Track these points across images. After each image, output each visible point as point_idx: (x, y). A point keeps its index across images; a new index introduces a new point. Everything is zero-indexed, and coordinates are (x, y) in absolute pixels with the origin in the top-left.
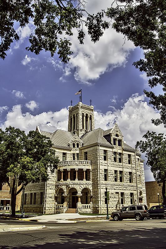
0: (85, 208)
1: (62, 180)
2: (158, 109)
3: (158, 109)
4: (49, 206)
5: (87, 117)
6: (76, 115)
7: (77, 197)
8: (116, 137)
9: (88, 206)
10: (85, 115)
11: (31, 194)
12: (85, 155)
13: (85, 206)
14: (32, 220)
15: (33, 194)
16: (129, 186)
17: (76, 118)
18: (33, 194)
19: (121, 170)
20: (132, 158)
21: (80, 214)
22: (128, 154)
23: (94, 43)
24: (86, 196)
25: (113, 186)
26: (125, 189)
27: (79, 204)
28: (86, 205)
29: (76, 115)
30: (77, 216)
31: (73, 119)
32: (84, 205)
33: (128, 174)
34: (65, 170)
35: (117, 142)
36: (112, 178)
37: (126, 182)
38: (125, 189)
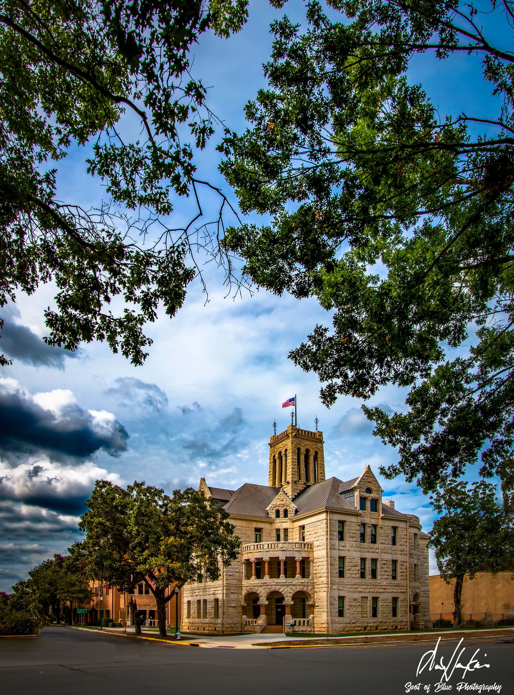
0: (300, 625)
1: (253, 577)
2: (394, 445)
3: (394, 445)
4: (231, 622)
5: (307, 457)
6: (283, 453)
7: (259, 606)
8: (366, 495)
9: (306, 622)
10: (303, 451)
11: (199, 601)
12: (300, 531)
13: (300, 621)
14: (191, 645)
15: (202, 602)
16: (360, 584)
17: (284, 458)
18: (202, 602)
19: (374, 556)
20: (400, 533)
21: (288, 635)
22: (392, 527)
23: (171, 317)
24: (302, 604)
25: (356, 586)
26: (382, 590)
27: (288, 619)
28: (302, 620)
29: (283, 453)
30: (282, 638)
31: (278, 462)
32: (298, 620)
33: (391, 563)
34: (260, 561)
35: (368, 504)
36: (355, 572)
37: (383, 577)
38: (382, 590)
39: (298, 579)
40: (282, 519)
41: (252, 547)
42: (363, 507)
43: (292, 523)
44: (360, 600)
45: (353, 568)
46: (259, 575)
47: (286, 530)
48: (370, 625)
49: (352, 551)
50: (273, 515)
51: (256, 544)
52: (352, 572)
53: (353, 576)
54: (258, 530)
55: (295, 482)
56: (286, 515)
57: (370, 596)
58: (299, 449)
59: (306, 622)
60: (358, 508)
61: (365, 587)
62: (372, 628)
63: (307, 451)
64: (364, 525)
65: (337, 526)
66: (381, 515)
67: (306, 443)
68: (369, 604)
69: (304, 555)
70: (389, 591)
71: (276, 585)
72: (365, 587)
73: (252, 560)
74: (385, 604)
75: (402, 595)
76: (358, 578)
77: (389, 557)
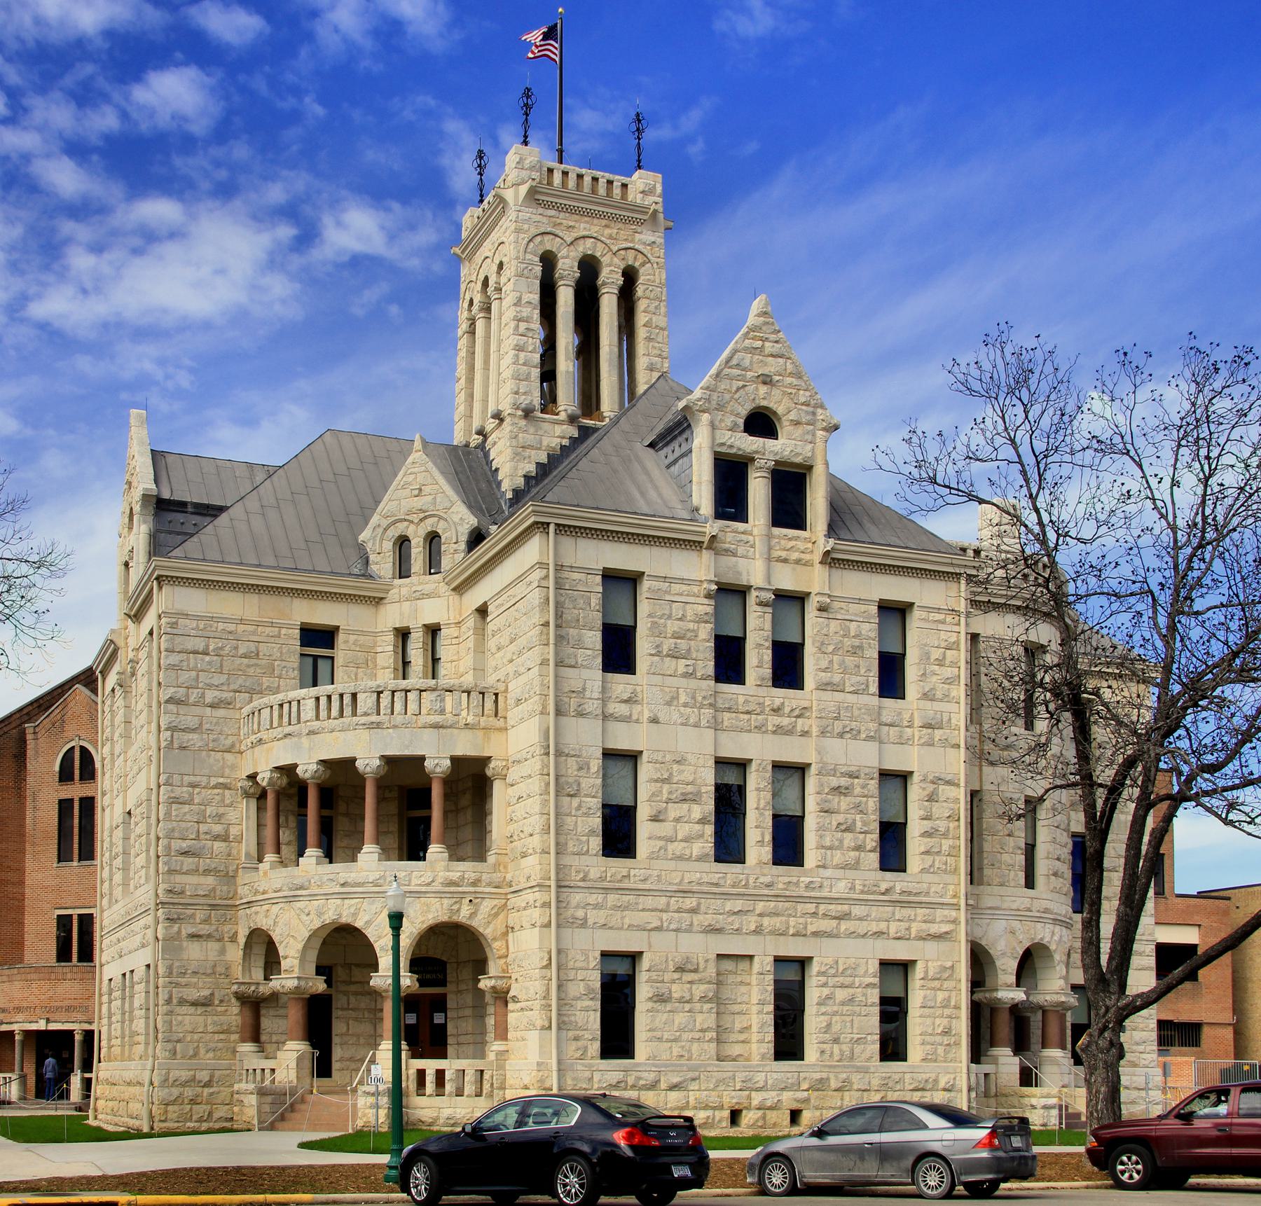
4: (185, 1075)
9: (470, 1077)
19: (791, 752)
20: (920, 641)
25: (690, 902)
35: (758, 491)
36: (684, 830)
40: (419, 580)
42: (731, 501)
43: (454, 598)
44: (711, 971)
45: (674, 811)
47: (433, 631)
48: (757, 1098)
49: (676, 725)
50: (383, 564)
52: (674, 828)
53: (676, 848)
54: (318, 638)
55: (528, 413)
56: (433, 564)
57: (765, 951)
58: (548, 261)
59: (470, 1077)
61: (738, 905)
62: (772, 1116)
63: (589, 267)
64: (731, 594)
65: (596, 600)
67: (583, 227)
69: (466, 746)
70: (862, 927)
71: (344, 896)
72: (738, 905)
74: (841, 995)
75: (931, 947)
76: (700, 859)
77: (868, 757)
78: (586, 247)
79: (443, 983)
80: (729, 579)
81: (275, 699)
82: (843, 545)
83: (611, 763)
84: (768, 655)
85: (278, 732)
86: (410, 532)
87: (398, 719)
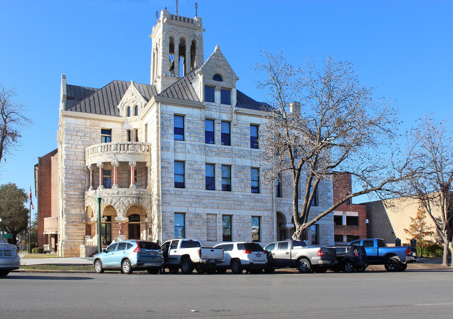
8: (214, 83)
19: (227, 161)
35: (218, 95)
39: (133, 189)
41: (99, 148)
46: (107, 185)
49: (194, 153)
51: (104, 144)
52: (195, 182)
60: (201, 99)
63: (183, 41)
64: (210, 120)
66: (234, 109)
68: (220, 224)
73: (99, 164)
78: (182, 35)
79: (139, 221)
80: (209, 117)
81: (92, 147)
82: (240, 109)
83: (69, 101)
84: (220, 137)
85: (92, 155)
86: (130, 105)
87: (122, 152)
